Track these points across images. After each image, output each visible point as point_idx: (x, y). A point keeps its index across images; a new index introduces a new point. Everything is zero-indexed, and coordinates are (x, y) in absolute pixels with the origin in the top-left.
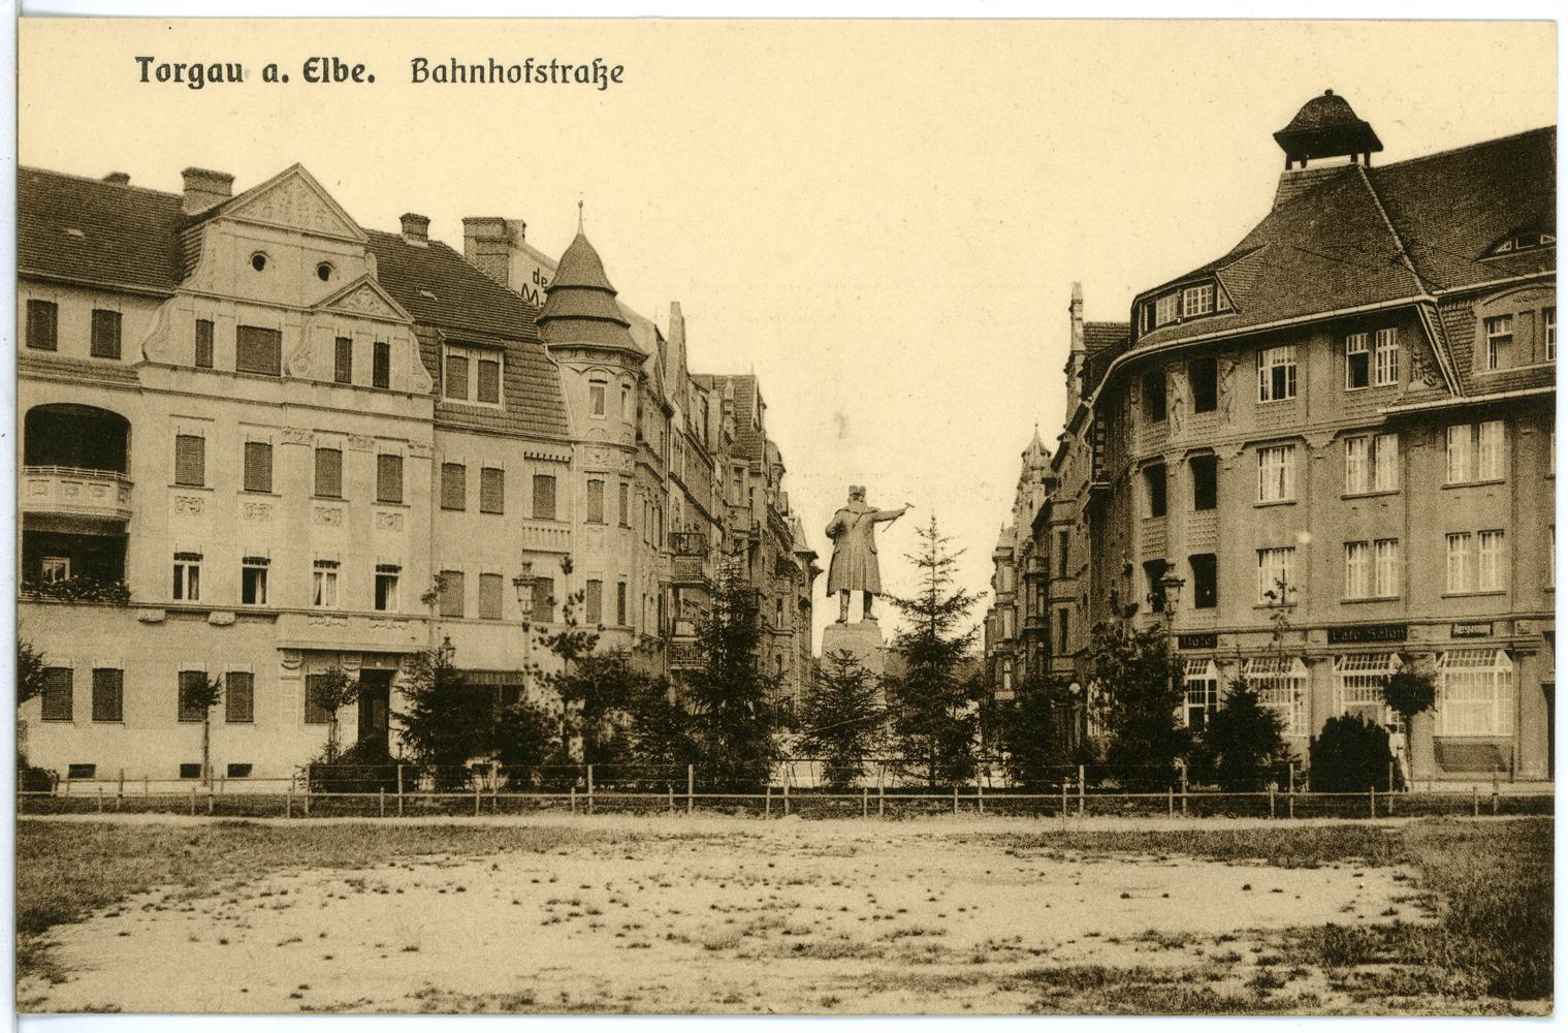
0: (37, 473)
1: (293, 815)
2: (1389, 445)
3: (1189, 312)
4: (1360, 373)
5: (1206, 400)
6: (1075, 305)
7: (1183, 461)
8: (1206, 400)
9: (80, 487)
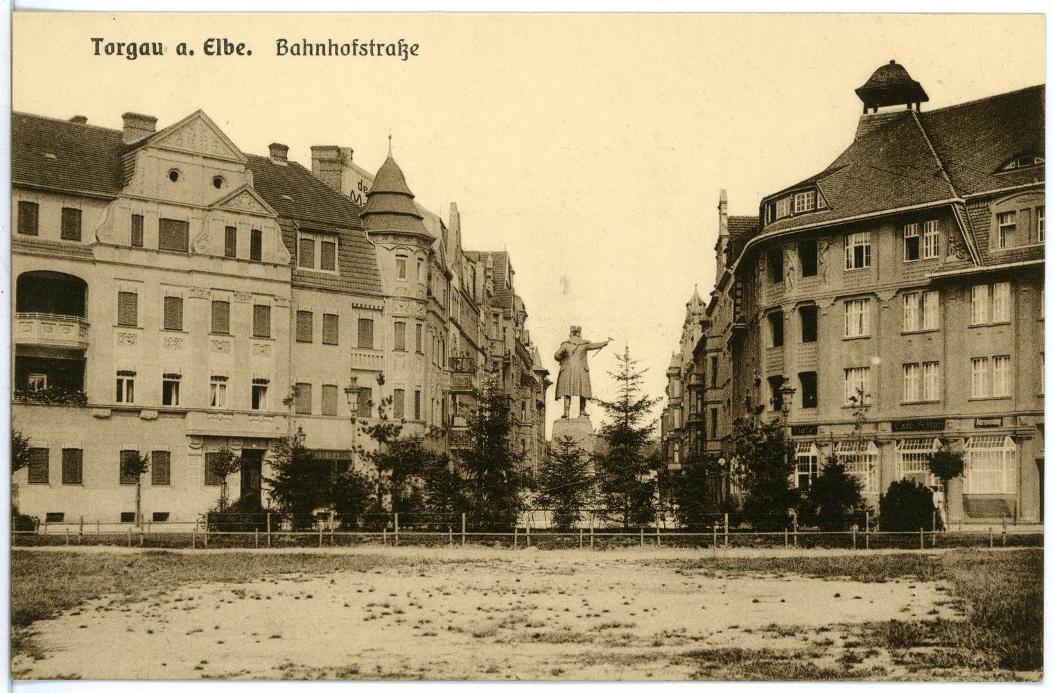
0: (25, 317)
1: (197, 547)
2: (933, 299)
3: (799, 209)
4: (913, 250)
5: (810, 268)
6: (722, 204)
7: (794, 309)
8: (810, 268)
9: (53, 326)
